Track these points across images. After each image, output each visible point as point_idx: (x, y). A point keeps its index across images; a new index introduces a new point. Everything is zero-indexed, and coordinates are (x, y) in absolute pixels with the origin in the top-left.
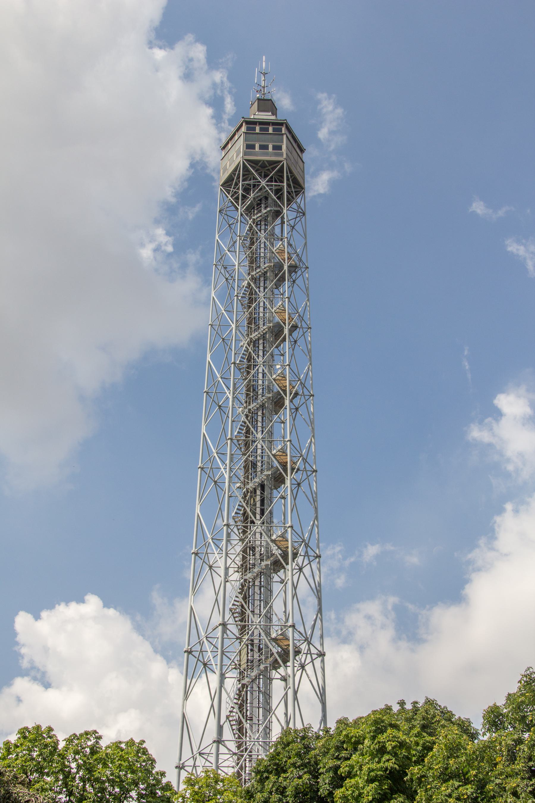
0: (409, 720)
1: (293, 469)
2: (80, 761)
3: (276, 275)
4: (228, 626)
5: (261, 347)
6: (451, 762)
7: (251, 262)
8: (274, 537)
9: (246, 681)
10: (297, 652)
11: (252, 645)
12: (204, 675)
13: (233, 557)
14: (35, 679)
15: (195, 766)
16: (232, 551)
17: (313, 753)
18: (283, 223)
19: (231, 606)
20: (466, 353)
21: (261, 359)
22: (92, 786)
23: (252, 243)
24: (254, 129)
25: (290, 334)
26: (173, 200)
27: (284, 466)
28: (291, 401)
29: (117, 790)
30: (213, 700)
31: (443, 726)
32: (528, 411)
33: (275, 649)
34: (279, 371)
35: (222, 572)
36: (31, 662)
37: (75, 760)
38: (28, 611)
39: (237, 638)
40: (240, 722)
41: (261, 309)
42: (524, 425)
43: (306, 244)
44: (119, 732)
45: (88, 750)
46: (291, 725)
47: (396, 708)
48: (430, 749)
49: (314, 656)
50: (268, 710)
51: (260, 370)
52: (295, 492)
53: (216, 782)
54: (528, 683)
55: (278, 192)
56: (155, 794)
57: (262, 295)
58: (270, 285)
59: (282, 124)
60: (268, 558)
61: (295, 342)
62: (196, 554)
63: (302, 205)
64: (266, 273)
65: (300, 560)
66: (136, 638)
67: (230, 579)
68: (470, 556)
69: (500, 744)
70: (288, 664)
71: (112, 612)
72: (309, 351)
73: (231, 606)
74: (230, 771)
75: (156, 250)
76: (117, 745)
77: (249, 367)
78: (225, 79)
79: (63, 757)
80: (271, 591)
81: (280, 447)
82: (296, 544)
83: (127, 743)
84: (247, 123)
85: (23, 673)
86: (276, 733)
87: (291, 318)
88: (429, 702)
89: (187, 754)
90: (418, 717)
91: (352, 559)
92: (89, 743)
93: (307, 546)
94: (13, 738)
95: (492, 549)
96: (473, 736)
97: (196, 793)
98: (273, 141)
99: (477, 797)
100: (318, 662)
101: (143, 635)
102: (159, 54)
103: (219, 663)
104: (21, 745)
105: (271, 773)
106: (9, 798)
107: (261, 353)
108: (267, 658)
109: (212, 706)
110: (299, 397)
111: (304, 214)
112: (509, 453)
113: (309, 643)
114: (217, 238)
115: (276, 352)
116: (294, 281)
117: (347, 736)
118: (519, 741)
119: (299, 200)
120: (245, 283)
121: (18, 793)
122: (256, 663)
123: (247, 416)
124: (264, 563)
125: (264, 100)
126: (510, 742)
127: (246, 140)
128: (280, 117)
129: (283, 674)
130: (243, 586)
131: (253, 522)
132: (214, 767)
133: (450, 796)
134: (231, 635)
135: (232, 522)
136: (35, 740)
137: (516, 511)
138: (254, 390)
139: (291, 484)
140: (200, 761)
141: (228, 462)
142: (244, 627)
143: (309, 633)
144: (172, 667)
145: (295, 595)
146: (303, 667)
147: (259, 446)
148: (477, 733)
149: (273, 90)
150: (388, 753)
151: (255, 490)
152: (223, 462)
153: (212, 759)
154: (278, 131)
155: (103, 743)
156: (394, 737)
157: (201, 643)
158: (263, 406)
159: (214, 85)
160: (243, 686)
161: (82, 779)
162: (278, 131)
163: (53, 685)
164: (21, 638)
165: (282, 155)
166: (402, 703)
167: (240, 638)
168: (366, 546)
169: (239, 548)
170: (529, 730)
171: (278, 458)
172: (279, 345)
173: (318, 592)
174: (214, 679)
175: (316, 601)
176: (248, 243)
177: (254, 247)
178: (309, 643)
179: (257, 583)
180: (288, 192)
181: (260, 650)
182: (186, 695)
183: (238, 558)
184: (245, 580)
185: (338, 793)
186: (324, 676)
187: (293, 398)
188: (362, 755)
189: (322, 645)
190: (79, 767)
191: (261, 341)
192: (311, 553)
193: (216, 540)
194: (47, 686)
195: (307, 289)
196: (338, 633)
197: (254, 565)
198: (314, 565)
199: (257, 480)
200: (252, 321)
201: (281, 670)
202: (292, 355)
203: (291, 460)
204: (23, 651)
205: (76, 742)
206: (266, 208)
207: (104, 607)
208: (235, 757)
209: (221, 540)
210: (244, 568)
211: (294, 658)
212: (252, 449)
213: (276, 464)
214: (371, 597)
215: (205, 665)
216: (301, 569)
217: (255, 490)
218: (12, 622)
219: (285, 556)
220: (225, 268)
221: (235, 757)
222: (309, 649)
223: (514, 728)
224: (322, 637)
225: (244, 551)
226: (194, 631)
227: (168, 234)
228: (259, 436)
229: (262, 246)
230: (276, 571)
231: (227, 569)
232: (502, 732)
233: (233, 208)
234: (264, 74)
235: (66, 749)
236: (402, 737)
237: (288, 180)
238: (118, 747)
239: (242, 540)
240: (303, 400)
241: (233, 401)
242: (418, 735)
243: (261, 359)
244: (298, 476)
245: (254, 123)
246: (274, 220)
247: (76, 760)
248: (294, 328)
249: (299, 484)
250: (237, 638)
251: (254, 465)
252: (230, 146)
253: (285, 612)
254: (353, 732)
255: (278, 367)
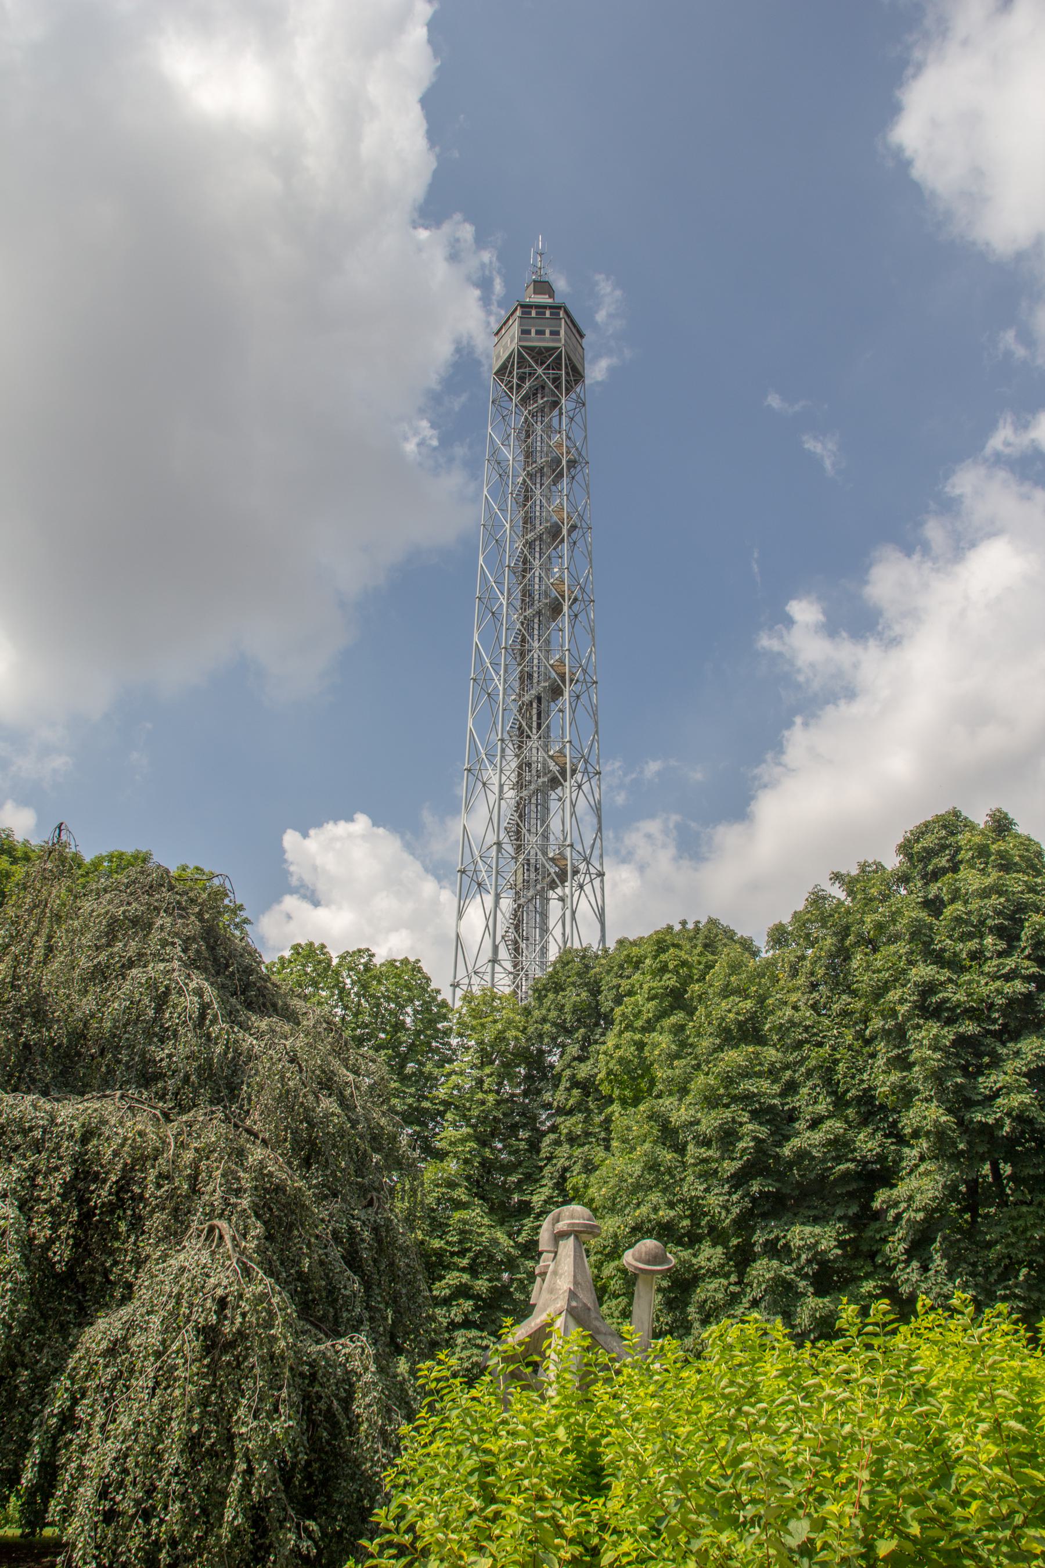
0: (691, 939)
1: (571, 681)
2: (354, 977)
3: (554, 471)
4: (504, 846)
5: (537, 549)
6: (732, 979)
7: (527, 457)
8: (551, 753)
9: (522, 901)
10: (576, 872)
11: (528, 865)
12: (478, 897)
13: (508, 773)
14: (304, 897)
15: (470, 984)
16: (507, 767)
17: (592, 972)
18: (561, 414)
19: (506, 825)
20: (756, 555)
21: (537, 561)
22: (367, 1001)
23: (528, 436)
24: (530, 313)
25: (569, 535)
26: (438, 388)
27: (562, 677)
28: (570, 607)
29: (393, 1006)
30: (487, 920)
31: (725, 945)
32: (821, 618)
33: (553, 870)
34: (557, 575)
35: (496, 790)
36: (301, 879)
37: (349, 976)
38: (295, 829)
39: (513, 858)
40: (516, 942)
41: (538, 508)
42: (816, 632)
43: (586, 437)
44: (390, 949)
45: (361, 967)
46: (569, 945)
47: (677, 927)
48: (713, 967)
49: (593, 876)
50: (545, 930)
51: (537, 574)
52: (574, 705)
53: (493, 1000)
54: (815, 901)
55: (556, 380)
56: (432, 1010)
57: (538, 492)
58: (547, 482)
59: (559, 308)
60: (545, 774)
61: (575, 543)
62: (469, 770)
63: (582, 395)
64: (543, 468)
65: (579, 776)
66: (407, 857)
67: (505, 796)
68: (756, 771)
69: (783, 960)
70: (566, 884)
71: (381, 831)
72: (590, 553)
73: (506, 825)
74: (507, 991)
75: (421, 444)
76: (392, 963)
77: (524, 570)
78: (494, 259)
79: (337, 973)
80: (548, 809)
81: (558, 657)
82: (574, 760)
83: (402, 962)
84: (523, 306)
85: (292, 891)
86: (553, 954)
87: (569, 518)
88: (713, 922)
89: (461, 973)
90: (701, 936)
91: (634, 776)
92: (362, 961)
93: (586, 762)
94: (287, 954)
95: (780, 764)
96: (755, 954)
97: (474, 1010)
98: (534, 326)
99: (756, 1012)
100: (597, 882)
101: (413, 854)
102: (423, 234)
103: (493, 883)
104: (295, 960)
105: (548, 991)
106: (287, 1009)
107: (537, 555)
108: (543, 878)
109: (487, 926)
110: (578, 603)
111: (584, 405)
112: (799, 663)
113: (588, 863)
114: (490, 430)
115: (554, 554)
116: (573, 478)
117: (628, 956)
118: (803, 958)
119: (578, 390)
120: (520, 480)
121: (295, 1005)
122: (532, 883)
123: (522, 623)
124: (540, 780)
125: (540, 282)
126: (792, 959)
127: (521, 325)
128: (558, 300)
129: (561, 894)
130: (518, 804)
131: (528, 737)
132: (489, 985)
133: (730, 1011)
134: (506, 855)
135: (506, 736)
136: (308, 956)
137: (806, 725)
138: (530, 595)
139: (570, 696)
140: (475, 980)
141: (502, 672)
142: (520, 846)
143: (588, 852)
144: (445, 888)
145: (573, 813)
146: (581, 887)
147: (536, 656)
148: (759, 951)
149: (550, 271)
150: (670, 972)
151: (531, 703)
152: (497, 673)
153: (488, 977)
154: (555, 315)
155: (378, 961)
156: (677, 956)
157: (476, 864)
158: (539, 613)
159: (483, 266)
160: (519, 906)
161: (357, 994)
162: (555, 315)
163: (322, 902)
164: (289, 856)
165: (559, 341)
166: (684, 923)
167: (516, 858)
168: (647, 763)
169: (514, 765)
170: (813, 947)
171: (556, 668)
172: (557, 546)
173: (597, 810)
174: (489, 900)
175: (595, 821)
176: (523, 436)
177: (529, 440)
178: (588, 863)
179: (533, 801)
180: (566, 381)
181: (536, 869)
182: (460, 915)
183: (513, 775)
184: (521, 798)
185: (618, 1011)
186: (603, 896)
187: (572, 604)
188: (643, 973)
189: (602, 864)
190: (353, 983)
191: (537, 543)
192: (590, 769)
193: (490, 756)
194: (316, 904)
195: (587, 486)
196: (617, 852)
197: (530, 782)
198: (594, 782)
199: (533, 692)
200: (527, 594)
201: (559, 890)
202: (571, 558)
203: (570, 671)
204: (292, 868)
205: (350, 959)
206: (542, 398)
207: (373, 825)
208: (512, 977)
209: (495, 756)
210: (520, 785)
211: (573, 879)
212: (527, 658)
213: (554, 675)
214: (652, 816)
215: (479, 885)
216: (579, 786)
217: (531, 703)
218: (280, 840)
219: (563, 772)
220: (499, 463)
221: (512, 977)
222: (588, 869)
223: (798, 944)
224: (601, 856)
225: (520, 767)
226: (467, 850)
227: (433, 426)
228: (536, 645)
229: (539, 439)
230: (553, 789)
231: (501, 786)
232: (786, 950)
233: (507, 398)
234: (541, 254)
235: (340, 965)
236: (684, 956)
237: (566, 367)
238: (393, 965)
239: (517, 756)
240: (583, 606)
241: (507, 608)
242: (701, 954)
243: (537, 561)
244: (577, 688)
245: (530, 307)
246: (551, 411)
247: (350, 977)
248: (573, 528)
249: (578, 697)
250: (513, 858)
251: (530, 676)
252: (503, 331)
253: (563, 831)
254: (635, 951)
255: (556, 570)
